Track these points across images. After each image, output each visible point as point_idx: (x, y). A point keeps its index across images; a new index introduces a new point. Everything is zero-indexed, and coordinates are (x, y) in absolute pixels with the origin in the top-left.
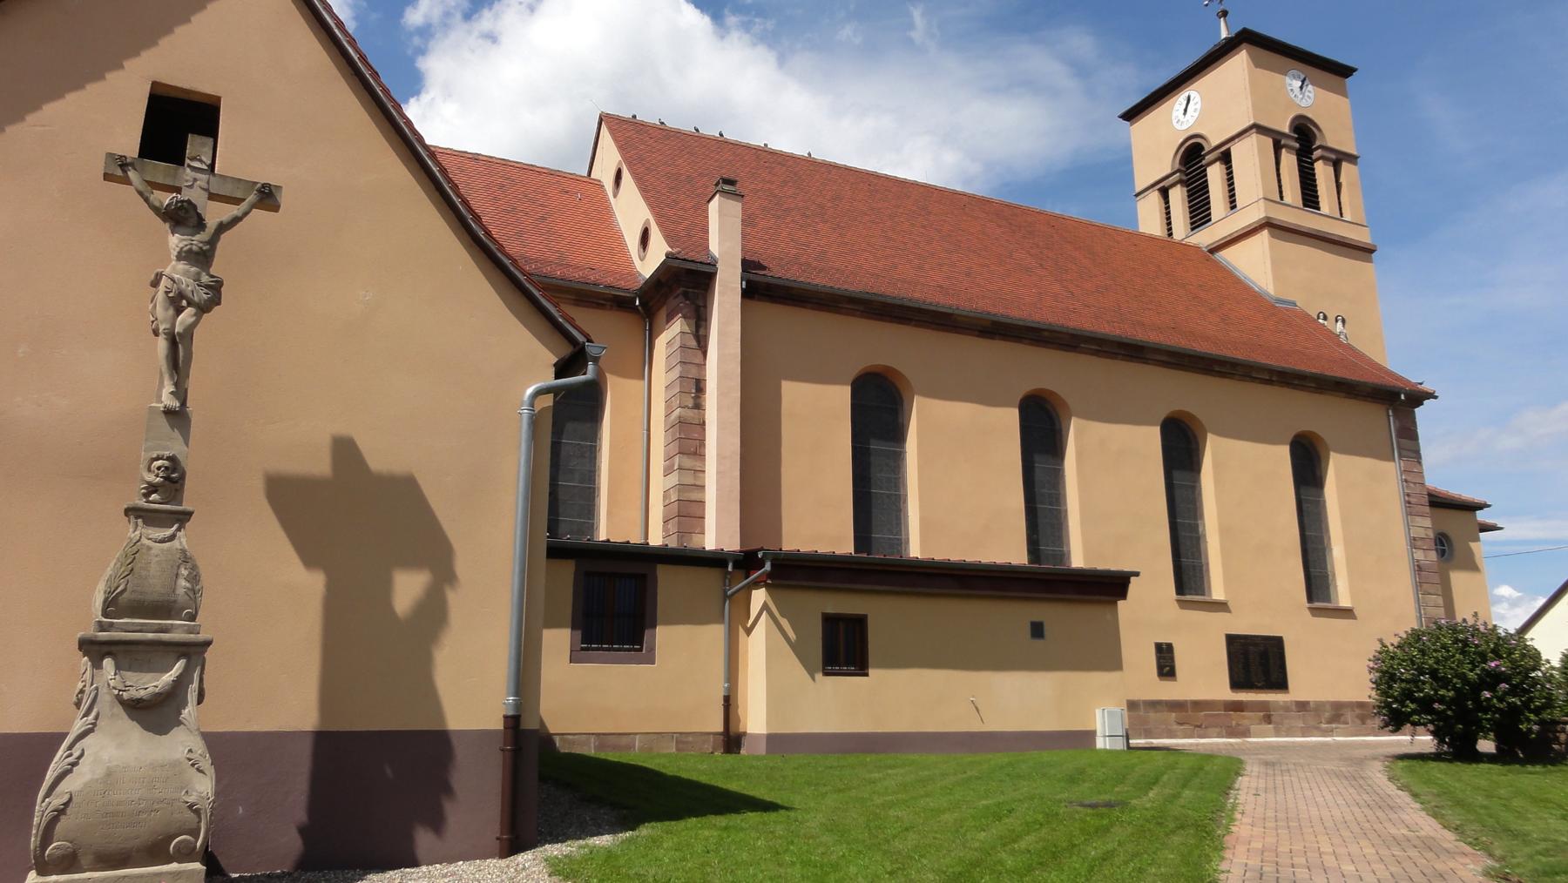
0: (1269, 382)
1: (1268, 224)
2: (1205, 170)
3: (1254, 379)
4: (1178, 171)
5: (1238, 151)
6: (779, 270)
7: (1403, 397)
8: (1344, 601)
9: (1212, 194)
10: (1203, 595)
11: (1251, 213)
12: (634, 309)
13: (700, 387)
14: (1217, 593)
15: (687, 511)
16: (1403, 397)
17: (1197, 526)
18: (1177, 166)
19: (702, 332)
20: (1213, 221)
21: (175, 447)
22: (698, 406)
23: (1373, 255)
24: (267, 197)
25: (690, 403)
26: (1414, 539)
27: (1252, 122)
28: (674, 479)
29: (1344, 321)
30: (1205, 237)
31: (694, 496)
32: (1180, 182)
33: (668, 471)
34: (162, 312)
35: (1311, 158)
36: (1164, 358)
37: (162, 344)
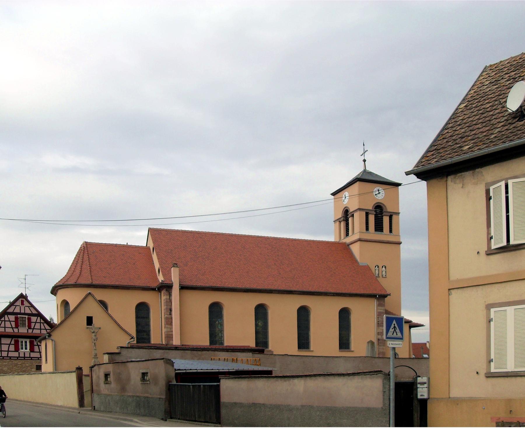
0: (334, 296)
1: (360, 240)
2: (349, 219)
3: (328, 295)
4: (343, 217)
5: (356, 215)
6: (187, 283)
7: (378, 296)
8: (352, 350)
9: (349, 227)
10: (110, 372)
11: (356, 237)
12: (156, 290)
13: (171, 310)
14: (311, 349)
15: (169, 337)
16: (378, 296)
17: (309, 333)
18: (343, 215)
19: (171, 298)
20: (349, 235)
21: (96, 352)
22: (171, 314)
23: (401, 245)
24: (100, 328)
25: (169, 314)
26: (378, 333)
27: (358, 208)
28: (166, 330)
29: (385, 267)
30: (348, 240)
31: (170, 333)
32: (344, 220)
33: (165, 327)
34: (93, 341)
35: (382, 215)
36: (300, 293)
37: (94, 344)
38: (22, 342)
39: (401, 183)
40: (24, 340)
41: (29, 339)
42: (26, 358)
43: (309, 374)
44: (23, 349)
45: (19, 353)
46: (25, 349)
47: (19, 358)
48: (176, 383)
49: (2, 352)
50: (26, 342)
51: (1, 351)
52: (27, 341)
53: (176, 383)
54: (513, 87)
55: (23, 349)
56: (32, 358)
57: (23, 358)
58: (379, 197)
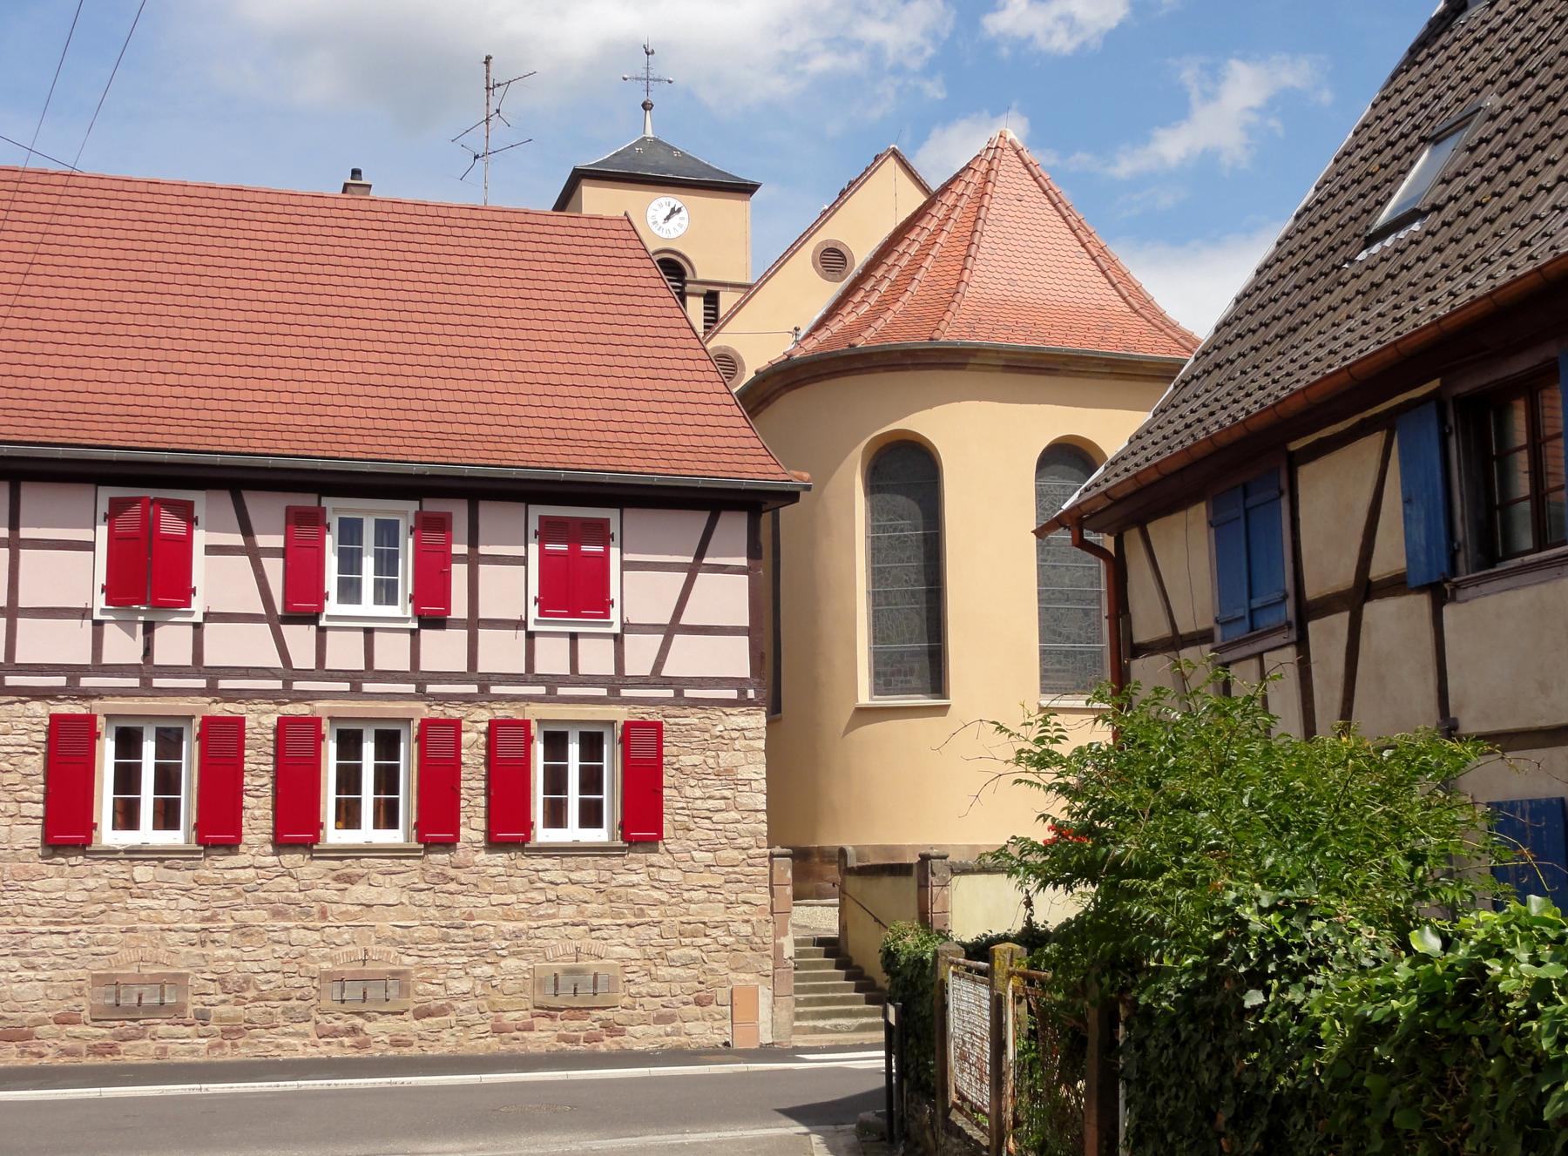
38: (351, 531)
39: (756, 180)
40: (370, 512)
41: (413, 506)
42: (157, 683)
43: (1108, 676)
44: (357, 599)
45: (322, 631)
46: (377, 601)
47: (368, 687)
48: (239, 722)
49: (483, 633)
50: (387, 532)
51: (12, 611)
52: (361, 521)
53: (239, 722)
54: (1415, 29)
55: (357, 599)
56: (484, 689)
57: (134, 682)
58: (661, 206)
